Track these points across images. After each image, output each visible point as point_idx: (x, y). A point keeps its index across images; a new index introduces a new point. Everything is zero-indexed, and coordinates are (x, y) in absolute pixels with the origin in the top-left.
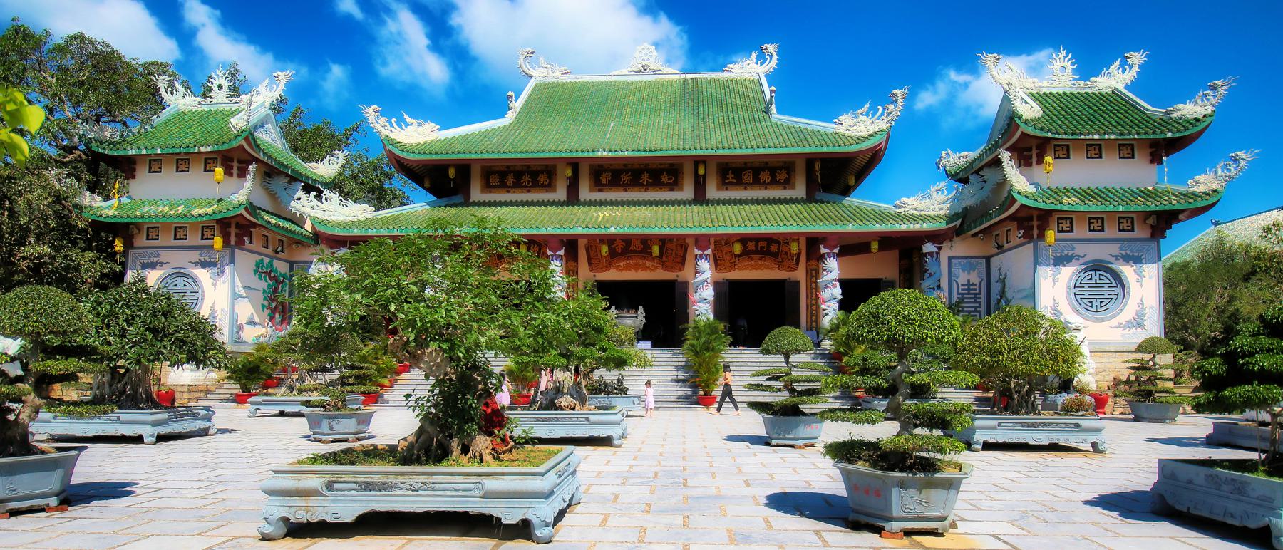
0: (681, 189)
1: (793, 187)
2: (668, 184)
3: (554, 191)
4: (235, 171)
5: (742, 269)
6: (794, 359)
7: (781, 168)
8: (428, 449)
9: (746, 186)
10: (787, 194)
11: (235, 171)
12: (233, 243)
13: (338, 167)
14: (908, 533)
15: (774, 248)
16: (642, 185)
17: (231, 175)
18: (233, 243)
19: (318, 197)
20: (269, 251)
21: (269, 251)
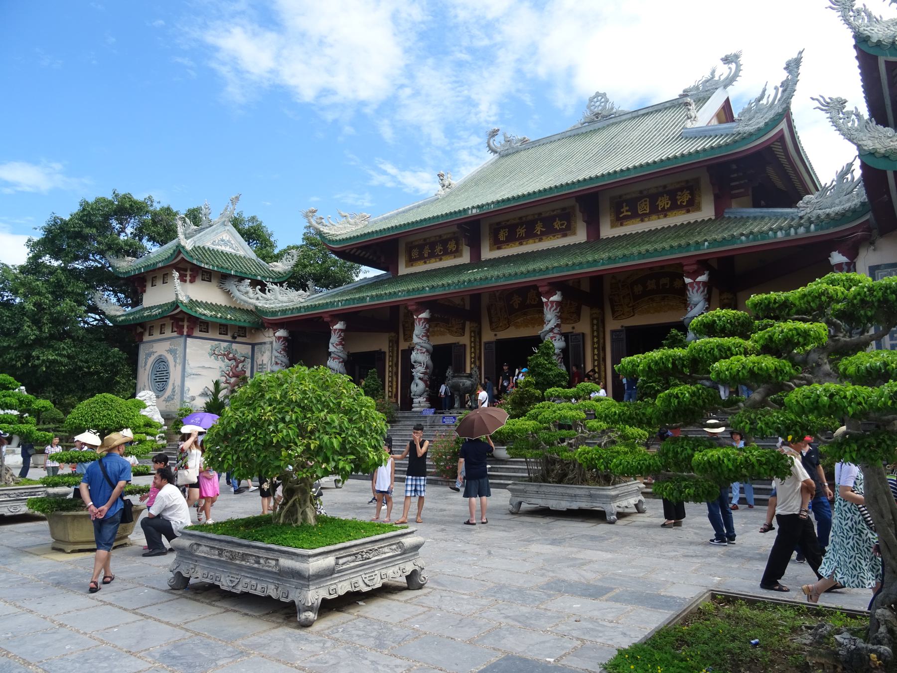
0: (574, 234)
1: (698, 209)
2: (561, 230)
3: (461, 256)
4: (188, 278)
5: (517, 326)
6: (117, 438)
7: (681, 189)
8: (520, 503)
9: (643, 218)
10: (692, 217)
11: (188, 278)
12: (185, 333)
13: (293, 262)
14: (328, 607)
15: (638, 289)
16: (536, 235)
17: (185, 281)
18: (185, 333)
19: (263, 291)
20: (228, 338)
21: (228, 338)
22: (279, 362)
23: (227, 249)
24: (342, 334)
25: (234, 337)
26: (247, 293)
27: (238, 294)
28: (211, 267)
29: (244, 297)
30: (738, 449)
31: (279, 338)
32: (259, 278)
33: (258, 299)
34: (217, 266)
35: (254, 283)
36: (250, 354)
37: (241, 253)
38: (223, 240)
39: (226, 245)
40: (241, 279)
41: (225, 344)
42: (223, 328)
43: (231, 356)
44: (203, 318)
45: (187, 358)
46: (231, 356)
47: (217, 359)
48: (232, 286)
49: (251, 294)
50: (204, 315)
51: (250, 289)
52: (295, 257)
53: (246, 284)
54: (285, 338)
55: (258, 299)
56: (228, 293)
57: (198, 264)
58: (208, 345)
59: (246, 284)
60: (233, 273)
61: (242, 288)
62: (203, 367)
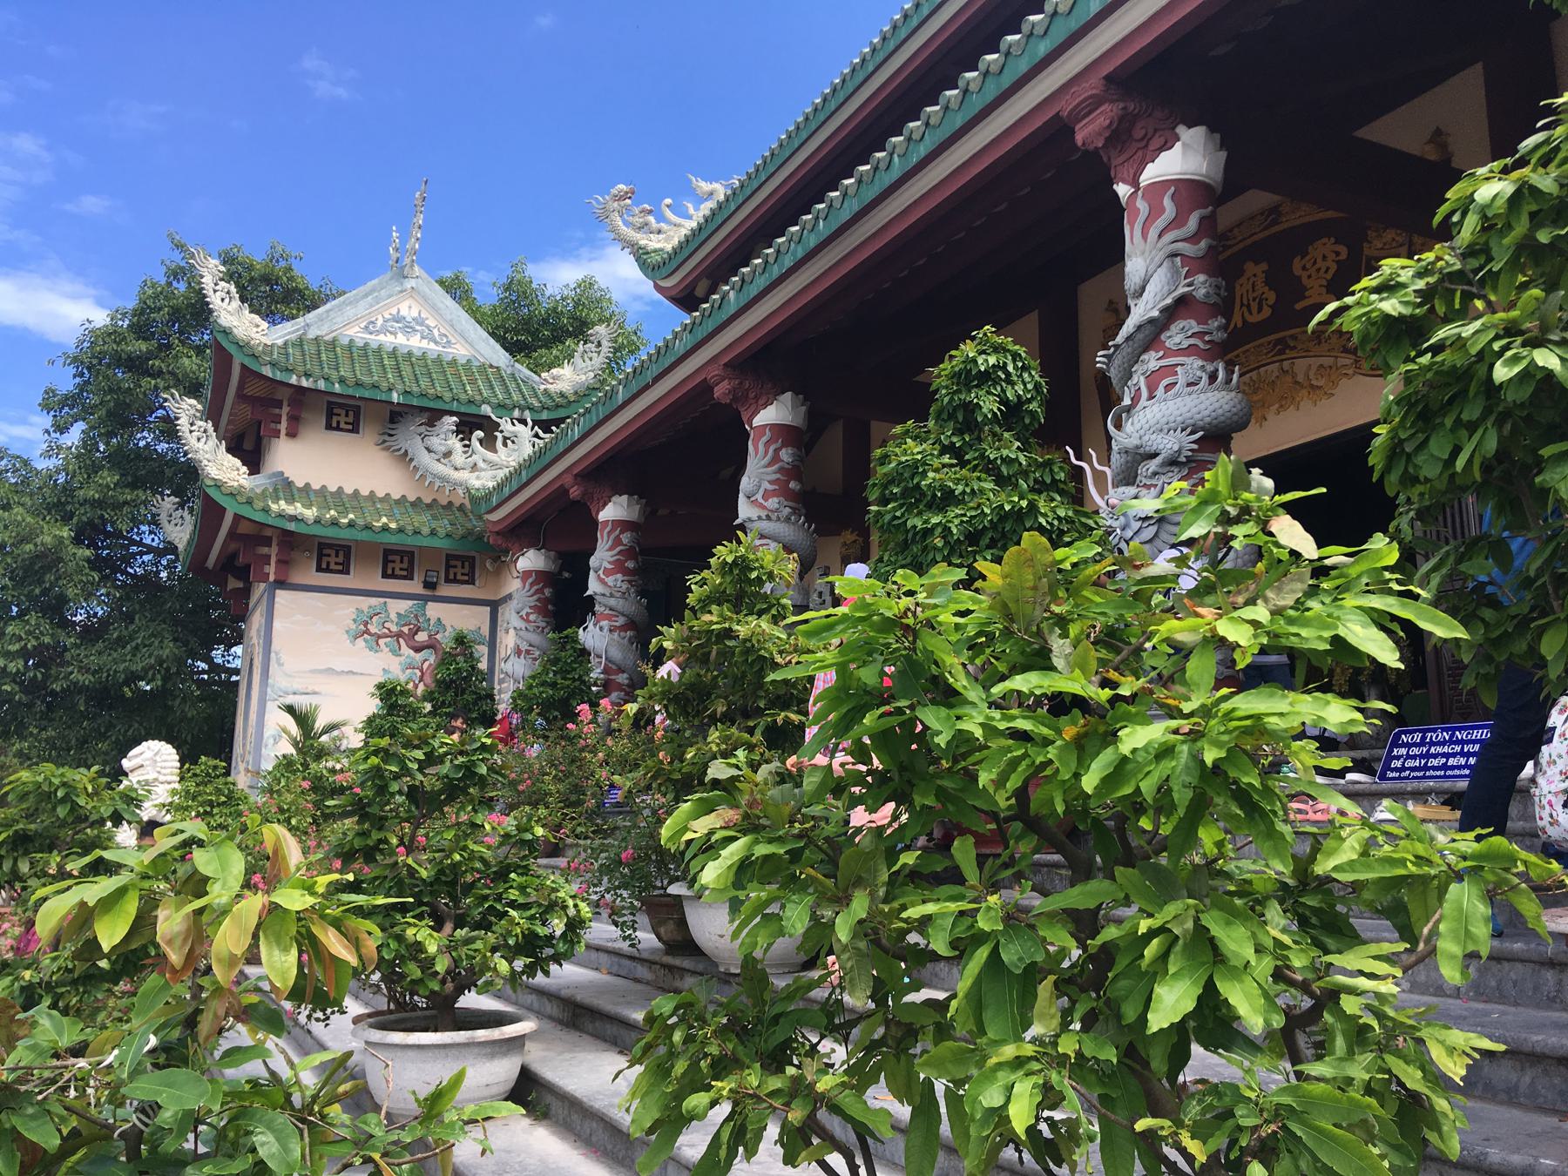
4: (283, 426)
13: (598, 361)
19: (489, 443)
22: (524, 646)
23: (416, 343)
24: (626, 538)
25: (429, 585)
26: (448, 454)
27: (425, 459)
28: (322, 385)
29: (441, 469)
30: (1020, 1152)
31: (526, 574)
32: (486, 410)
33: (474, 467)
34: (342, 381)
35: (469, 425)
36: (486, 631)
37: (460, 351)
38: (398, 319)
39: (408, 329)
40: (433, 416)
41: (404, 606)
42: (396, 560)
43: (422, 637)
44: (292, 526)
45: (275, 646)
46: (422, 637)
47: (375, 646)
48: (410, 438)
49: (459, 457)
50: (294, 518)
51: (455, 443)
52: (605, 343)
53: (445, 435)
54: (542, 577)
55: (474, 467)
56: (405, 458)
57: (279, 376)
58: (346, 609)
59: (445, 435)
60: (395, 397)
61: (435, 442)
62: (330, 671)
